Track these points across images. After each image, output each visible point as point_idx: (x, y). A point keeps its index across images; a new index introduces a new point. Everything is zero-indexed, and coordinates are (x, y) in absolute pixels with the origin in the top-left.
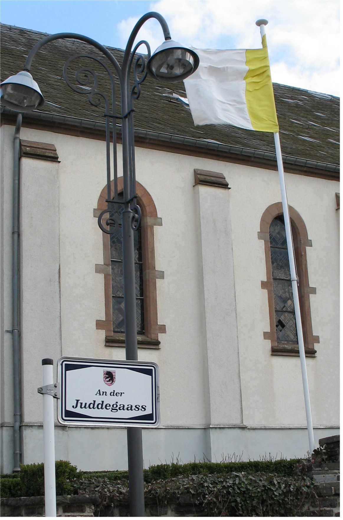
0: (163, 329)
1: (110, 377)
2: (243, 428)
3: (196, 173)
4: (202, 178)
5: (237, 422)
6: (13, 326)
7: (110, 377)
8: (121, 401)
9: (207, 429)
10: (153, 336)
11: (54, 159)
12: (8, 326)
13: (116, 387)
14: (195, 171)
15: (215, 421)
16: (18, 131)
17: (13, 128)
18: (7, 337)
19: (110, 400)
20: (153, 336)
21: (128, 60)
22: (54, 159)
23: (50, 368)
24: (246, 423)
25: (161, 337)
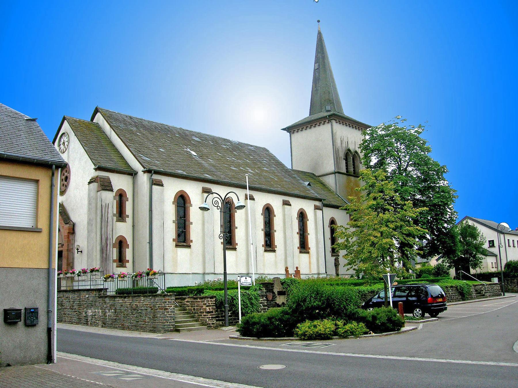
0: (192, 241)
1: (246, 278)
2: (215, 274)
3: (203, 188)
4: (205, 190)
5: (213, 272)
6: (150, 241)
7: (246, 278)
8: (248, 282)
9: (204, 274)
10: (189, 244)
11: (162, 185)
12: (148, 241)
13: (247, 280)
14: (203, 188)
15: (207, 272)
16: (151, 176)
17: (151, 174)
18: (148, 244)
19: (246, 282)
20: (189, 244)
21: (328, 354)
22: (162, 185)
23: (239, 277)
24: (216, 272)
25: (191, 244)
